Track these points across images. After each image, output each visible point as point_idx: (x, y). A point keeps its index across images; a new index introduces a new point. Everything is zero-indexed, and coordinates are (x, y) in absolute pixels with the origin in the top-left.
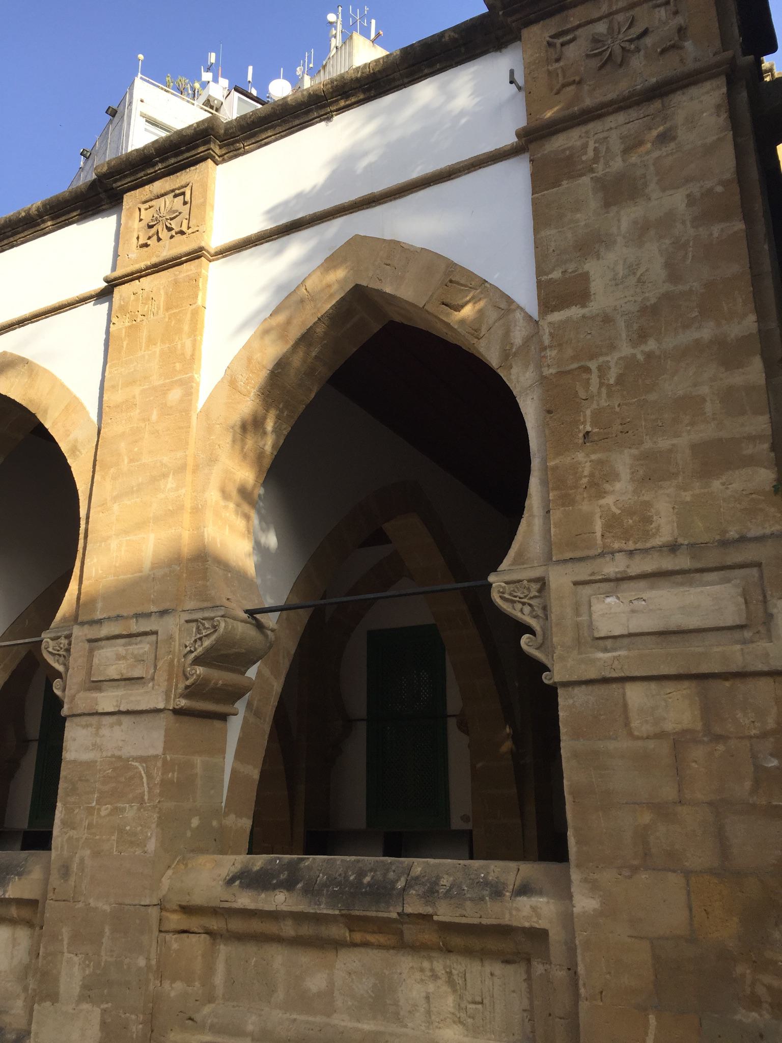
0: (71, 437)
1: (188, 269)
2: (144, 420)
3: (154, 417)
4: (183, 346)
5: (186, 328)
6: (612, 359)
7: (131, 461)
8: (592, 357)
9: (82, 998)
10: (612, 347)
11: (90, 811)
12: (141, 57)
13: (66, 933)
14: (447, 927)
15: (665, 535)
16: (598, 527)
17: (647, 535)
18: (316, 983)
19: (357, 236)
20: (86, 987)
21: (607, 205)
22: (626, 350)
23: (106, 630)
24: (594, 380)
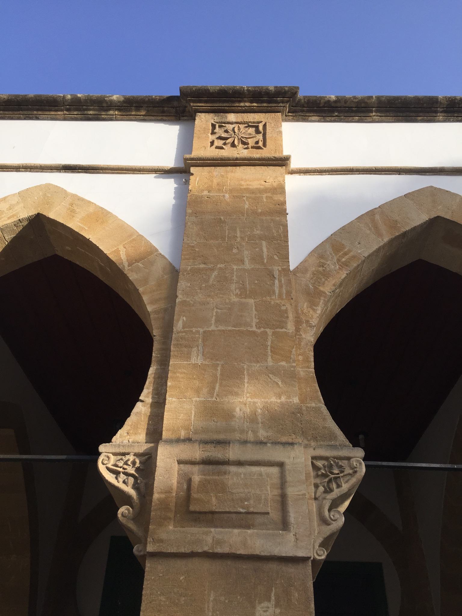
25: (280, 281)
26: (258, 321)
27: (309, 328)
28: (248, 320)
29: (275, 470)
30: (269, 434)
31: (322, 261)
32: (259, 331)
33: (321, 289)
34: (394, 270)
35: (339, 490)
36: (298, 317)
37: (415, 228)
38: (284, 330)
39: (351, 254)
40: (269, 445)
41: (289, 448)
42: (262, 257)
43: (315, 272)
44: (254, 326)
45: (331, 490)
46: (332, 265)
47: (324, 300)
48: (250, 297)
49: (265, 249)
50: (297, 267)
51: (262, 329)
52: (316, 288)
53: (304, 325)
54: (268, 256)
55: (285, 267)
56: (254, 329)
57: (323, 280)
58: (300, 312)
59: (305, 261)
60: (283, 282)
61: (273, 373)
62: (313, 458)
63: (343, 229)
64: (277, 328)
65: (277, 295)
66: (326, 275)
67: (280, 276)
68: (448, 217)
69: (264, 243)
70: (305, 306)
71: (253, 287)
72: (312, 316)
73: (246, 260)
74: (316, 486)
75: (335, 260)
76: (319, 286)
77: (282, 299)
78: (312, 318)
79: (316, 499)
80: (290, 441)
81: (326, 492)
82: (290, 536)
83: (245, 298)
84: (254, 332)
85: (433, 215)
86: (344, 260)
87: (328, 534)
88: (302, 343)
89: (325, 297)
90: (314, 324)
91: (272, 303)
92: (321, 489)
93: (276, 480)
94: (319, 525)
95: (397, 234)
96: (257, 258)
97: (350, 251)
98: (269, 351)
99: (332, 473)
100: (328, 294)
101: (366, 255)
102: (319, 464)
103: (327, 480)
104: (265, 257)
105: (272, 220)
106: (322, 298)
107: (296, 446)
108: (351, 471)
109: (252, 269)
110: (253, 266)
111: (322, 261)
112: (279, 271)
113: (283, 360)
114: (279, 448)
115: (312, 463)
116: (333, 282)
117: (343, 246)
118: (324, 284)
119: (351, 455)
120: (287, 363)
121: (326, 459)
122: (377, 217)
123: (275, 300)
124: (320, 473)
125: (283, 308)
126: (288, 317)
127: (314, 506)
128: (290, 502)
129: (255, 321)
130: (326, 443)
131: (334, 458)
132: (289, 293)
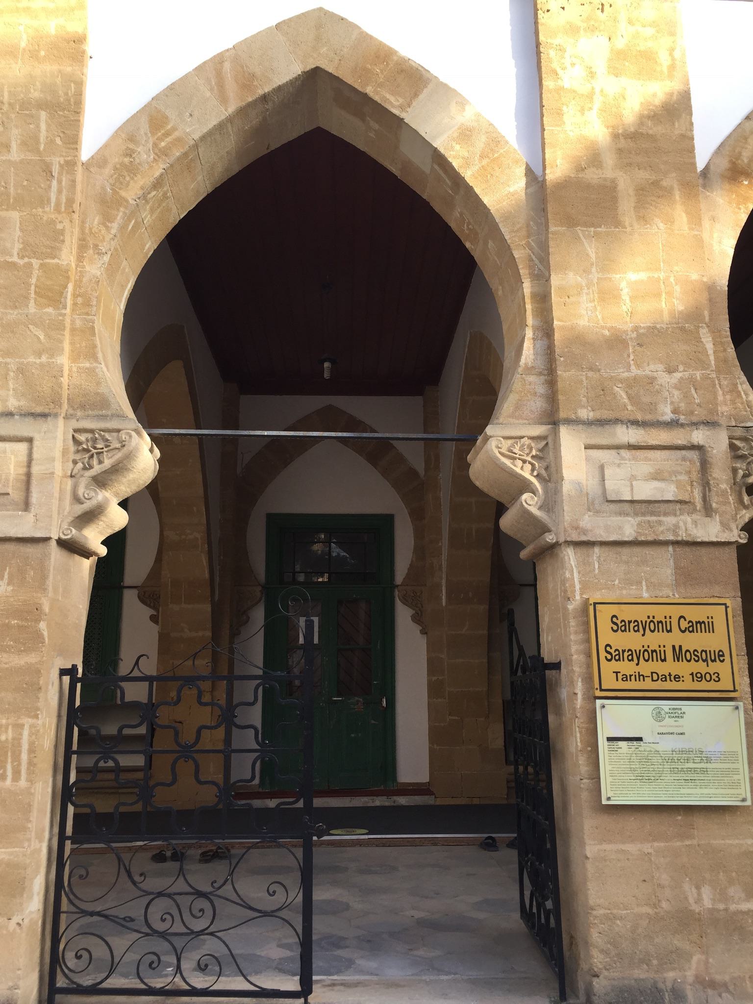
25: (60, 182)
26: (21, 246)
27: (96, 256)
28: (8, 245)
29: (23, 447)
30: (22, 403)
31: (131, 146)
32: (21, 262)
33: (123, 193)
34: (273, 147)
35: (100, 466)
36: (84, 240)
37: (280, 88)
38: (56, 261)
39: (177, 134)
40: (16, 417)
41: (40, 421)
42: (38, 142)
43: (118, 166)
44: (15, 253)
45: (91, 467)
46: (144, 155)
47: (124, 213)
48: (14, 209)
49: (43, 126)
50: (92, 157)
51: (26, 260)
52: (115, 192)
53: (91, 251)
54: (47, 137)
55: (69, 158)
56: (15, 259)
57: (128, 178)
58: (87, 231)
59: (106, 146)
60: (64, 183)
61: (35, 325)
62: (75, 431)
63: (171, 88)
64: (47, 257)
65: (53, 205)
66: (132, 169)
67: (60, 174)
68: (330, 70)
69: (43, 115)
70: (96, 222)
71: (19, 191)
72: (104, 238)
73: (14, 146)
74: (75, 462)
75: (150, 146)
76: (120, 189)
77: (59, 212)
78: (103, 240)
79: (71, 476)
80: (47, 411)
81: (85, 468)
82: (30, 517)
83: (7, 210)
84: (14, 264)
85: (310, 66)
86: (163, 144)
87: (79, 513)
88: (84, 279)
89: (126, 208)
90: (104, 251)
91: (45, 218)
92: (80, 465)
93: (24, 458)
94: (71, 504)
95: (250, 100)
96: (30, 143)
97: (174, 129)
98: (32, 292)
99: (95, 448)
100: (132, 202)
101: (196, 136)
102: (82, 437)
103: (87, 456)
104: (42, 140)
105: (60, 71)
106: (122, 209)
107: (49, 418)
108: (118, 445)
109: (22, 161)
110: (22, 157)
111: (131, 146)
112: (61, 166)
113: (49, 306)
114: (30, 420)
115: (73, 436)
116: (142, 183)
117: (165, 119)
118: (128, 184)
119: (120, 427)
120: (55, 309)
121: (92, 431)
122: (227, 66)
123: (48, 213)
124: (80, 448)
125: (59, 226)
126: (63, 241)
127: (69, 483)
128: (34, 482)
129: (18, 246)
130: (96, 412)
131: (100, 430)
132: (70, 201)
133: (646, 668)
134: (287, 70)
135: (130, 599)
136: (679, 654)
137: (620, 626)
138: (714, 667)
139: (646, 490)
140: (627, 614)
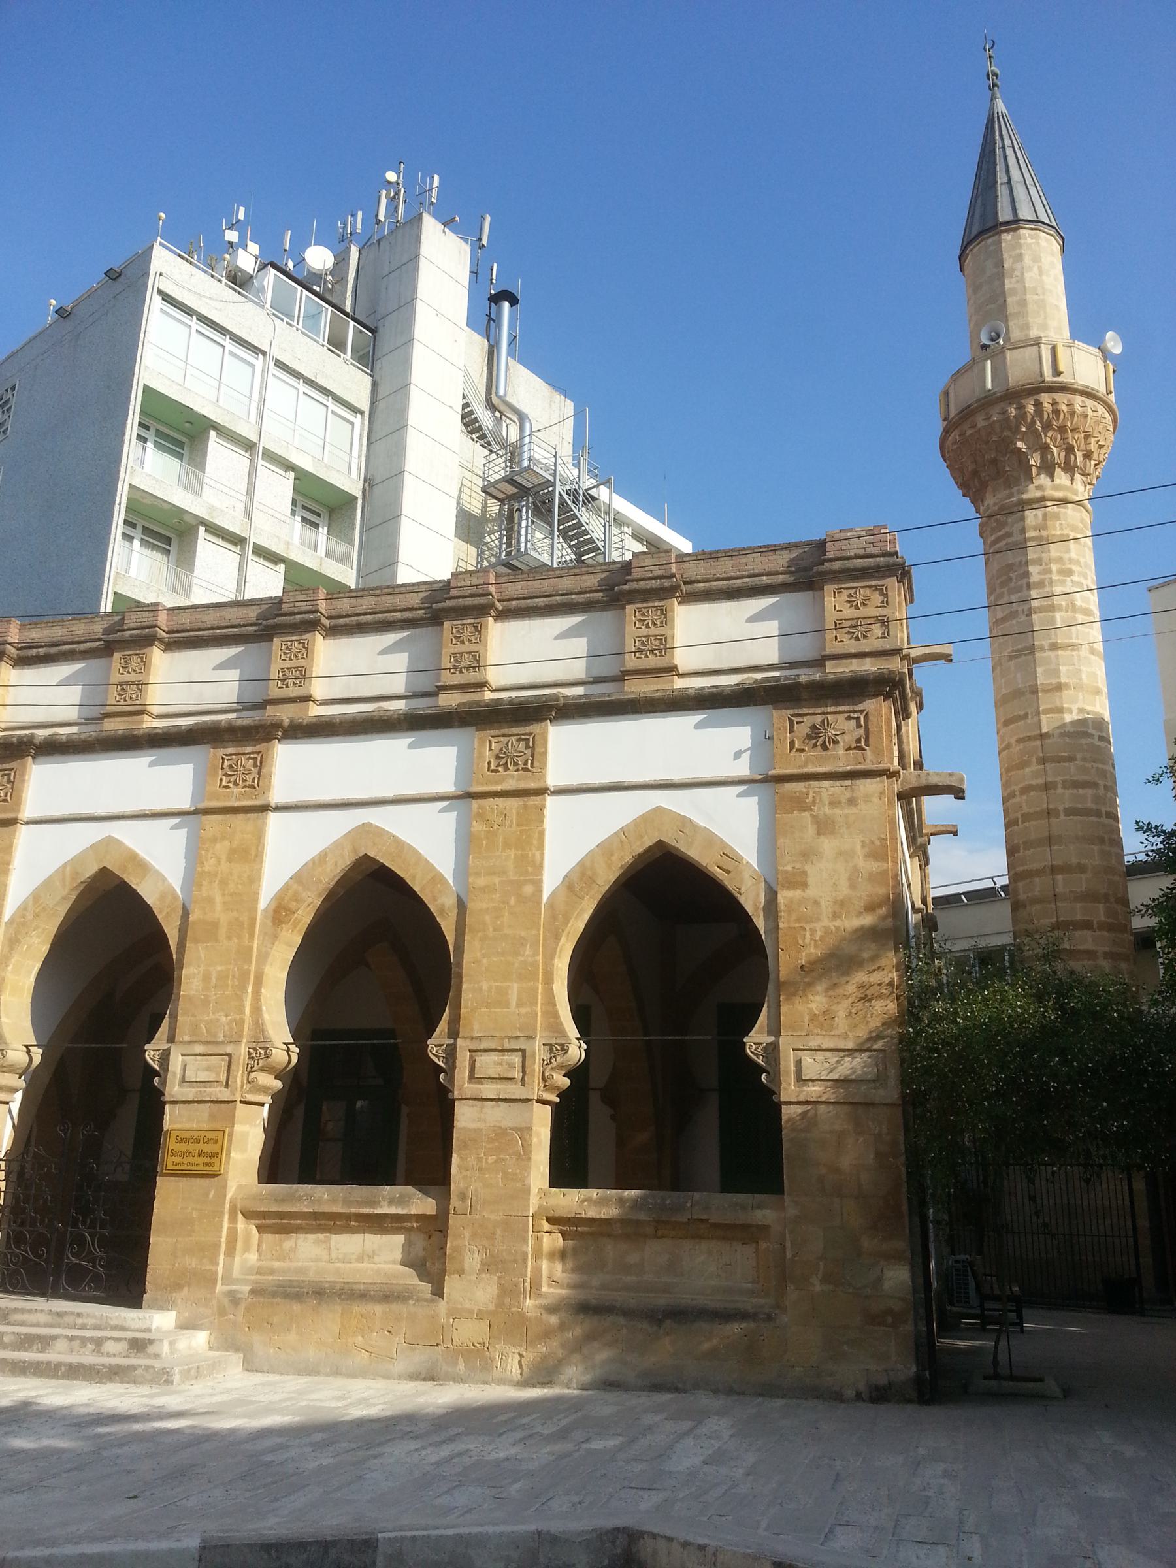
0: (439, 901)
1: (533, 801)
2: (504, 902)
3: (512, 901)
4: (534, 855)
5: (535, 842)
6: (818, 926)
7: (495, 930)
8: (807, 922)
9: (481, 1271)
10: (818, 919)
11: (479, 1160)
12: (163, 215)
13: (467, 1234)
14: (716, 1226)
15: (841, 1031)
16: (806, 1020)
17: (832, 1028)
18: (633, 1258)
19: (659, 807)
20: (482, 1264)
21: (819, 834)
22: (825, 922)
23: (483, 1046)
24: (808, 935)
133: (186, 1160)
134: (91, 869)
135: (594, 1098)
136: (200, 1154)
137: (179, 1141)
138: (213, 1160)
139: (203, 1076)
140: (183, 1135)
